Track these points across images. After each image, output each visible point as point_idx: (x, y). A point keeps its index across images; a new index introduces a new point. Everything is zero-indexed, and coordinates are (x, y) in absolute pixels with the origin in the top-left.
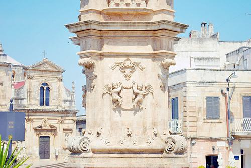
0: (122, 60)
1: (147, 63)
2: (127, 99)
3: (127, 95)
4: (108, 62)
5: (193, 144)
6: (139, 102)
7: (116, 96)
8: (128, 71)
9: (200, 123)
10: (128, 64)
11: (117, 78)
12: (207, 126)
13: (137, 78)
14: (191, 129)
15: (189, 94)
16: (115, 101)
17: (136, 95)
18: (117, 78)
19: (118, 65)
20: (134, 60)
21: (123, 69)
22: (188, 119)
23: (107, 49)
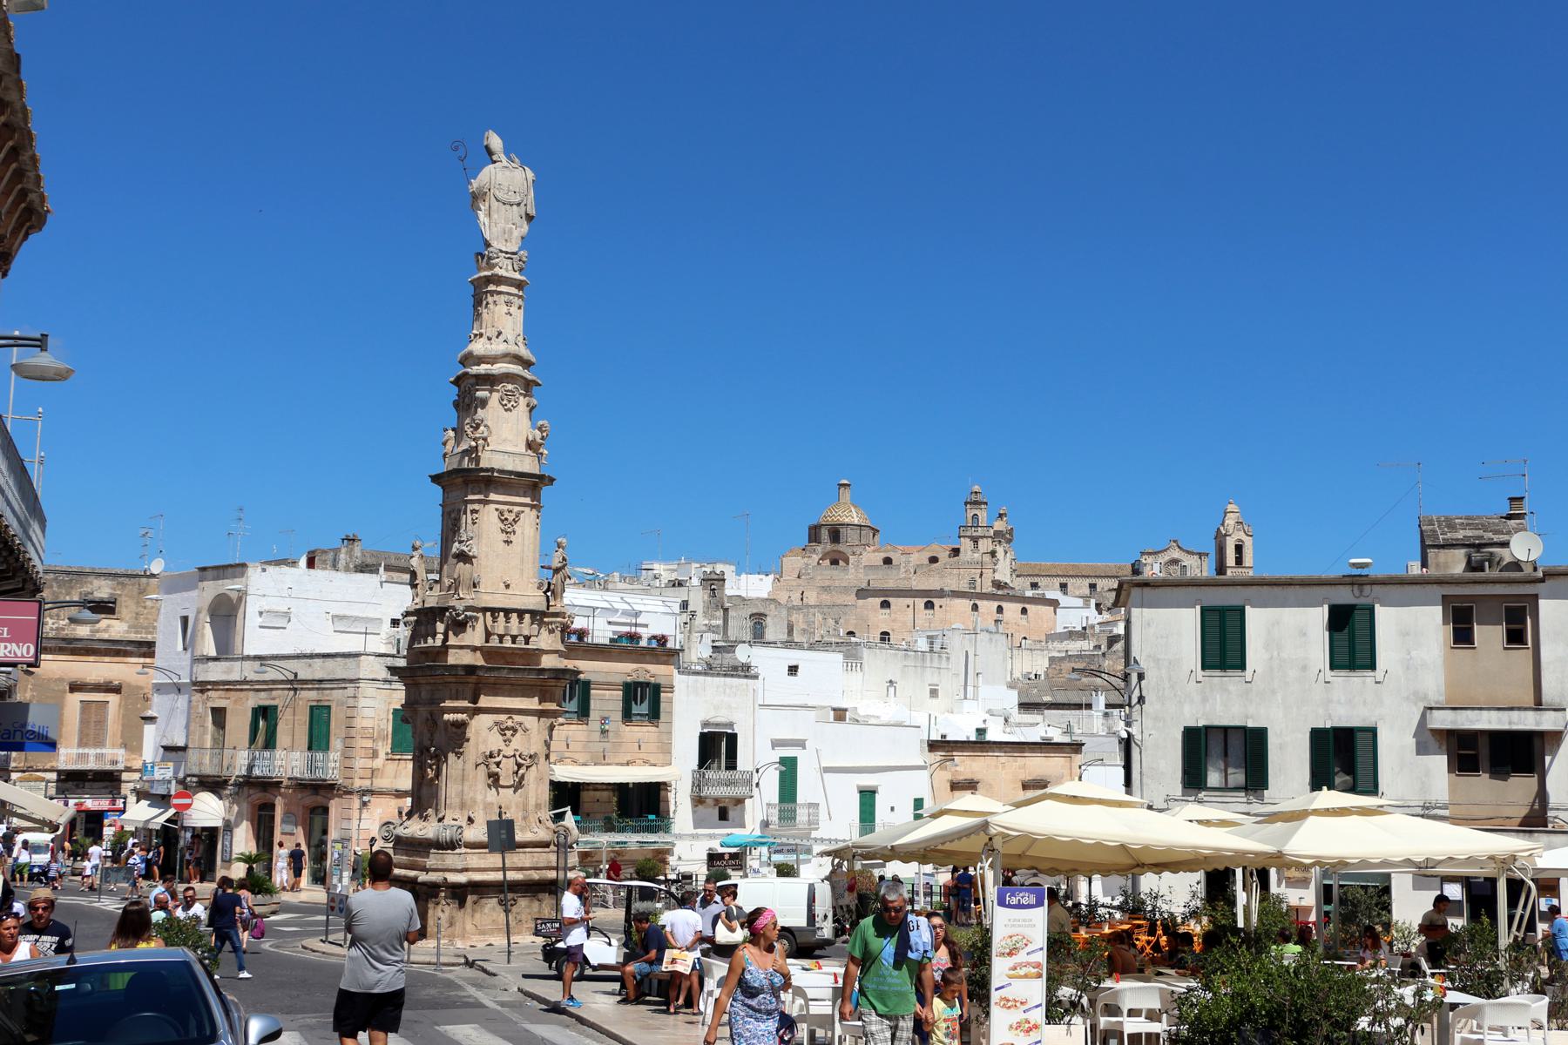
0: (503, 717)
1: (530, 722)
2: (506, 770)
3: (508, 766)
4: (484, 720)
5: (365, 804)
6: (522, 777)
7: (494, 768)
8: (509, 733)
9: (378, 763)
10: (510, 723)
11: (494, 742)
12: (392, 766)
13: (518, 742)
14: (361, 773)
15: (362, 702)
16: (490, 775)
17: (519, 766)
18: (494, 742)
19: (497, 724)
20: (517, 718)
21: (503, 731)
22: (358, 753)
23: (484, 701)
